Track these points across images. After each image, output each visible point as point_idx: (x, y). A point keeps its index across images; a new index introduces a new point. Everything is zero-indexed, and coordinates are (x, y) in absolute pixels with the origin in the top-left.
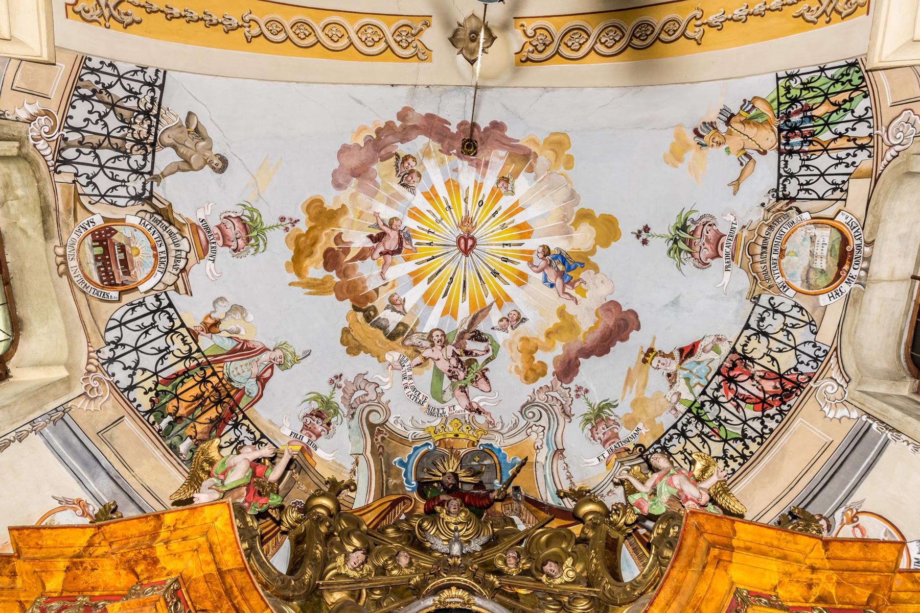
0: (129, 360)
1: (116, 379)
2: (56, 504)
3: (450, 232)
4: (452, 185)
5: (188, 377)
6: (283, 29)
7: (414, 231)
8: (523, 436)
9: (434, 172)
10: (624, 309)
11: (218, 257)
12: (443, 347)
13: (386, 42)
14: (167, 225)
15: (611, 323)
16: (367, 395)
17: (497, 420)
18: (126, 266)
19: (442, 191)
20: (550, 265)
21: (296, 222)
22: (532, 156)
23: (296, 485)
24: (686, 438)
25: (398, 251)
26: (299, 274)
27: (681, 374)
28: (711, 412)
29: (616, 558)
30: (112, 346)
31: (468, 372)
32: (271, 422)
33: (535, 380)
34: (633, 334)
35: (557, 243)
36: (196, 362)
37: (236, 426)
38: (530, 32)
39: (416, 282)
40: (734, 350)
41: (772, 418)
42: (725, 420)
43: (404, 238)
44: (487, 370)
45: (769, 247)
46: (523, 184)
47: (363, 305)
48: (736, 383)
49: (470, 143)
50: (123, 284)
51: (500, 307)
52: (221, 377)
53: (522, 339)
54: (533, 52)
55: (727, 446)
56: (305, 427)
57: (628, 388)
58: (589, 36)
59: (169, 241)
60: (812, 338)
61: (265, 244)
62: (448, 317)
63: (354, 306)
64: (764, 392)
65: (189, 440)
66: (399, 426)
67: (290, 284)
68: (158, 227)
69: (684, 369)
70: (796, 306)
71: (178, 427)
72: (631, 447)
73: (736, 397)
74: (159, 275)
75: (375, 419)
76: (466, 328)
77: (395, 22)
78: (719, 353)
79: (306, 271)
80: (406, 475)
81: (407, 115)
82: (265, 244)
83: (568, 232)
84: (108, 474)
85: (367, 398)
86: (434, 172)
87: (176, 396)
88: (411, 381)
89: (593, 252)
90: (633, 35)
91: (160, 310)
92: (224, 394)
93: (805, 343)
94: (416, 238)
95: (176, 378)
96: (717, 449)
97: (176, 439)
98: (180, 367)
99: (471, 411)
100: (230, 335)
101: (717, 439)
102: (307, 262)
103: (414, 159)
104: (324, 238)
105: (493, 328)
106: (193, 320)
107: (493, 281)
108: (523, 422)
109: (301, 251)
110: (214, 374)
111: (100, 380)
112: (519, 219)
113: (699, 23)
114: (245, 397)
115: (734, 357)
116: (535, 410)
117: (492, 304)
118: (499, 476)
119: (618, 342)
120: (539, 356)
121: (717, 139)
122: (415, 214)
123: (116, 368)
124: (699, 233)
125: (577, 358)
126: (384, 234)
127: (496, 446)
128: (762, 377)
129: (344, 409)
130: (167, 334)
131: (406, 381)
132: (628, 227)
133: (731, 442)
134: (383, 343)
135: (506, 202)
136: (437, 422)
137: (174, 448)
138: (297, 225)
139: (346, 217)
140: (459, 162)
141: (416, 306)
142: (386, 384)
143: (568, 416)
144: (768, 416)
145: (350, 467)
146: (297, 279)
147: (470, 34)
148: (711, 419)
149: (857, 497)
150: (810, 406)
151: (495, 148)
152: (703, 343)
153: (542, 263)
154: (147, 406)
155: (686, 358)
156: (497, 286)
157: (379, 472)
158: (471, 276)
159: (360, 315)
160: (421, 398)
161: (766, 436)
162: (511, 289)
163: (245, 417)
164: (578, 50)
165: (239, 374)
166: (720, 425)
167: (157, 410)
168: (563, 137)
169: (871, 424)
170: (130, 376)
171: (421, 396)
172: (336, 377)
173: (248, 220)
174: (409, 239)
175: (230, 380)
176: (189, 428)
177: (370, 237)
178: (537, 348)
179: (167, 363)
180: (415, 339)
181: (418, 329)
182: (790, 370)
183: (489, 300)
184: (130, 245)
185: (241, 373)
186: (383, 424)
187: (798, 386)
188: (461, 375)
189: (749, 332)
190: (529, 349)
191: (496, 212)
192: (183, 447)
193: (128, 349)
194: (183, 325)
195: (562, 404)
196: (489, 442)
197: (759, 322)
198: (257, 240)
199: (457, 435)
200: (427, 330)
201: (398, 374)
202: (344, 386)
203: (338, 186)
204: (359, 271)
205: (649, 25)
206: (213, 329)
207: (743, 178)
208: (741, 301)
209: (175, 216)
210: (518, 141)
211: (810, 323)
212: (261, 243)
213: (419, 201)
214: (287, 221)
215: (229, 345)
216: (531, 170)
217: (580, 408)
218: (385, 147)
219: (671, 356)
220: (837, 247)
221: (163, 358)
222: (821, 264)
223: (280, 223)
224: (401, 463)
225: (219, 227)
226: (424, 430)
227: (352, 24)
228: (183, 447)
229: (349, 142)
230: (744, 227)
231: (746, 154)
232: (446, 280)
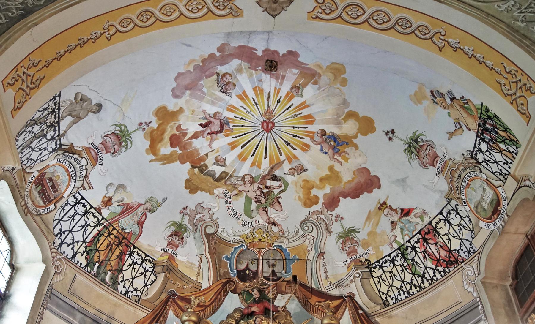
0: (69, 240)
1: (66, 254)
3: (257, 118)
4: (258, 90)
5: (100, 236)
6: (132, 21)
7: (231, 119)
8: (300, 241)
10: (372, 174)
11: (104, 162)
12: (251, 184)
13: (208, 8)
14: (72, 155)
18: (55, 188)
19: (251, 94)
20: (326, 141)
21: (149, 123)
22: (317, 75)
23: (169, 281)
25: (221, 132)
26: (155, 154)
27: (399, 225)
28: (411, 255)
30: (59, 236)
32: (149, 246)
33: (311, 206)
34: (375, 190)
35: (330, 129)
36: (103, 226)
37: (130, 255)
39: (233, 148)
40: (430, 223)
43: (224, 124)
44: (280, 197)
45: (462, 177)
46: (309, 91)
47: (198, 163)
49: (271, 64)
50: (55, 198)
51: (290, 162)
52: (118, 229)
53: (304, 181)
54: (321, 13)
56: (169, 243)
57: (368, 223)
58: (365, 13)
59: (74, 163)
60: (471, 239)
61: (131, 143)
63: (192, 166)
64: (440, 256)
65: (109, 273)
66: (225, 235)
67: (150, 162)
68: (67, 159)
71: (102, 268)
72: (363, 260)
73: (425, 252)
75: (210, 231)
76: (267, 173)
78: (423, 221)
79: (159, 150)
80: (230, 266)
81: (225, 48)
82: (131, 143)
83: (339, 123)
84: (79, 311)
85: (204, 218)
86: (245, 82)
87: (97, 250)
88: (231, 205)
89: (356, 137)
90: (397, 22)
91: (77, 203)
92: (121, 238)
95: (95, 239)
96: (408, 277)
97: (103, 275)
98: (95, 232)
99: (269, 224)
102: (159, 145)
103: (230, 75)
104: (169, 129)
105: (285, 174)
106: (96, 202)
107: (286, 147)
108: (301, 232)
109: (155, 139)
110: (114, 229)
111: (59, 260)
113: (442, 37)
114: (133, 236)
116: (309, 225)
117: (285, 160)
118: (285, 268)
119: (365, 193)
120: (314, 192)
122: (232, 108)
123: (64, 247)
124: (425, 148)
125: (338, 197)
126: (210, 122)
127: (284, 247)
128: (441, 247)
129: (190, 228)
130: (84, 215)
131: (228, 205)
132: (381, 127)
133: (416, 276)
134: (211, 183)
135: (297, 101)
136: (248, 231)
137: (103, 280)
138: (150, 125)
139: (183, 115)
142: (216, 207)
143: (329, 232)
144: (438, 270)
146: (154, 158)
148: (410, 258)
150: (458, 277)
151: (290, 68)
152: (415, 211)
153: (320, 140)
154: (84, 263)
155: (404, 216)
157: (214, 264)
158: (271, 145)
160: (237, 215)
161: (434, 281)
162: (298, 152)
163: (135, 247)
164: (356, 18)
165: (127, 224)
166: (413, 264)
167: (90, 263)
168: (341, 66)
169: (479, 305)
171: (238, 214)
172: (184, 209)
173: (119, 132)
174: (228, 124)
175: (123, 229)
176: (108, 265)
177: (201, 125)
178: (313, 187)
180: (233, 180)
181: (235, 175)
182: (455, 250)
183: (283, 158)
185: (127, 223)
186: (215, 234)
187: (457, 262)
188: (263, 200)
189: (441, 217)
190: (308, 187)
191: (290, 107)
192: (107, 278)
193: (67, 233)
194: (92, 207)
195: (326, 223)
196: (280, 244)
197: (448, 214)
198: (126, 142)
199: (260, 240)
200: (241, 175)
201: (223, 201)
202: (189, 213)
203: (176, 96)
205: (408, 21)
206: (108, 204)
207: (455, 134)
208: (441, 197)
209: (75, 148)
210: (308, 65)
211: (472, 231)
213: (235, 101)
214: (144, 124)
215: (119, 210)
216: (316, 83)
217: (337, 228)
218: (209, 69)
219: (396, 211)
220: (494, 203)
221: (85, 230)
222: (485, 205)
223: (139, 127)
225: (102, 143)
226: (240, 236)
228: (107, 278)
229: (182, 70)
231: (459, 123)
232: (254, 146)
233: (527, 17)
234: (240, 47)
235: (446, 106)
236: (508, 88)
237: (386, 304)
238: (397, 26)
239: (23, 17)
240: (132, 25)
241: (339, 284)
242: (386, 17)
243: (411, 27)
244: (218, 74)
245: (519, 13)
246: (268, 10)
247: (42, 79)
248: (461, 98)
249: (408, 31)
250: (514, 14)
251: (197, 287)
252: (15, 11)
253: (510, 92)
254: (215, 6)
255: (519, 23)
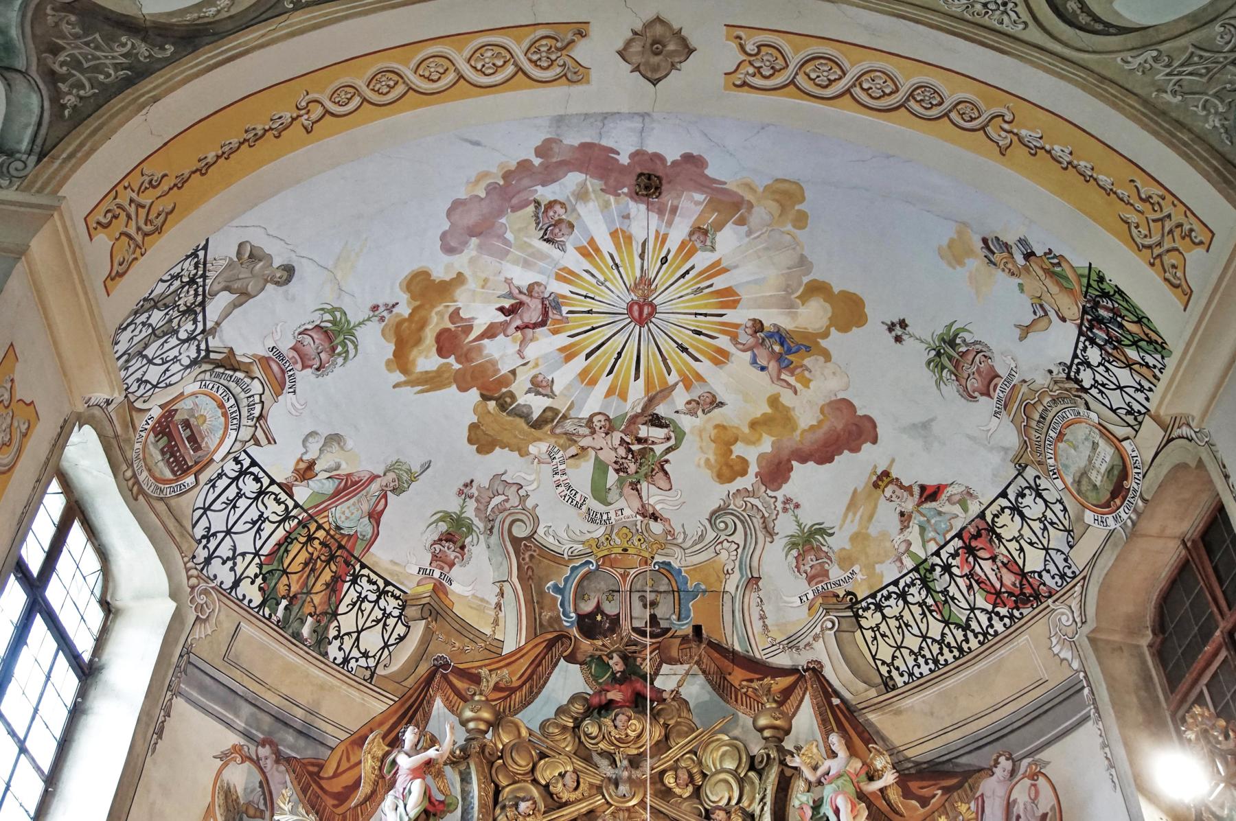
0: (225, 551)
2: (219, 763)
3: (618, 296)
4: (621, 237)
7: (564, 297)
8: (710, 553)
9: (594, 220)
13: (515, 64)
15: (840, 426)
16: (507, 500)
17: (678, 529)
18: (196, 441)
19: (606, 245)
20: (762, 344)
21: (393, 306)
24: (906, 602)
25: (543, 323)
26: (405, 371)
27: (917, 519)
29: (786, 796)
31: (641, 464)
33: (731, 480)
34: (867, 447)
35: (772, 318)
38: (750, 48)
39: (568, 358)
40: (982, 515)
41: (1001, 619)
42: (953, 598)
43: (550, 306)
44: (667, 461)
46: (728, 240)
47: (495, 391)
48: (975, 557)
49: (649, 183)
50: (196, 463)
51: (688, 387)
53: (717, 426)
55: (947, 630)
56: (435, 557)
57: (850, 514)
60: (1066, 549)
61: (356, 347)
62: (615, 398)
63: (482, 396)
66: (551, 539)
67: (394, 387)
68: (222, 381)
69: (922, 514)
70: (1060, 502)
74: (234, 433)
75: (520, 531)
77: (527, 35)
78: (966, 510)
80: (562, 604)
82: (356, 347)
85: (508, 505)
86: (594, 220)
87: (285, 572)
88: (565, 477)
89: (826, 335)
90: (911, 95)
91: (243, 473)
93: (1058, 550)
94: (566, 304)
96: (936, 629)
98: (280, 533)
99: (645, 517)
100: (328, 475)
101: (939, 617)
102: (415, 352)
104: (434, 318)
108: (711, 535)
109: (404, 342)
110: (320, 527)
111: (205, 592)
112: (720, 283)
113: (1006, 126)
115: (982, 525)
117: (676, 384)
120: (739, 450)
121: (1010, 266)
122: (565, 275)
123: (216, 567)
124: (970, 357)
125: (789, 461)
126: (521, 304)
127: (676, 565)
128: (1005, 565)
129: (479, 524)
130: (256, 499)
131: (557, 477)
132: (878, 313)
134: (522, 431)
135: (702, 260)
136: (599, 531)
137: (297, 635)
138: (395, 310)
139: (463, 288)
140: (632, 204)
141: (569, 387)
142: (532, 482)
143: (770, 533)
144: (997, 614)
145: (494, 600)
146: (402, 378)
147: (652, 45)
148: (938, 589)
149: (1044, 755)
153: (751, 341)
154: (257, 599)
155: (926, 500)
156: (685, 363)
157: (529, 602)
158: (648, 350)
159: (492, 404)
160: (578, 498)
162: (704, 367)
163: (363, 566)
164: (826, 87)
165: (347, 518)
166: (946, 602)
167: (269, 599)
169: (1083, 687)
170: (232, 569)
171: (578, 496)
172: (466, 485)
173: (329, 325)
174: (557, 307)
175: (338, 528)
177: (501, 309)
179: (265, 534)
180: (569, 426)
181: (572, 414)
182: (1034, 572)
183: (673, 378)
184: (193, 416)
185: (348, 516)
186: (530, 537)
187: (1037, 596)
188: (632, 468)
190: (725, 439)
191: (687, 272)
192: (306, 631)
193: (220, 536)
194: (273, 482)
195: (763, 516)
196: (667, 559)
197: (1018, 496)
198: (344, 345)
200: (585, 414)
201: (547, 469)
202: (476, 494)
203: (449, 250)
204: (486, 352)
206: (309, 474)
207: (1034, 328)
208: (1004, 460)
209: (239, 359)
210: (725, 183)
211: (1069, 531)
212: (350, 346)
213: (572, 259)
214: (381, 309)
215: (330, 487)
216: (742, 222)
217: (785, 526)
218: (518, 192)
219: (909, 489)
221: (259, 530)
224: (557, 589)
225: (293, 348)
226: (583, 543)
227: (460, 50)
228: (306, 631)
229: (463, 195)
230: (1025, 381)
231: (1041, 306)
233: (1184, 83)
234: (584, 146)
235: (1013, 269)
236: (1145, 232)
237: (888, 685)
238: (912, 103)
239: (128, 83)
240: (356, 101)
241: (791, 643)
242: (889, 82)
243: (940, 104)
244: (537, 204)
245: (1167, 75)
246: (642, 68)
247: (168, 214)
248: (1045, 254)
249: (935, 112)
250: (1157, 77)
251: (493, 649)
252: (111, 72)
253: (1147, 242)
254: (530, 60)
255: (1168, 97)
